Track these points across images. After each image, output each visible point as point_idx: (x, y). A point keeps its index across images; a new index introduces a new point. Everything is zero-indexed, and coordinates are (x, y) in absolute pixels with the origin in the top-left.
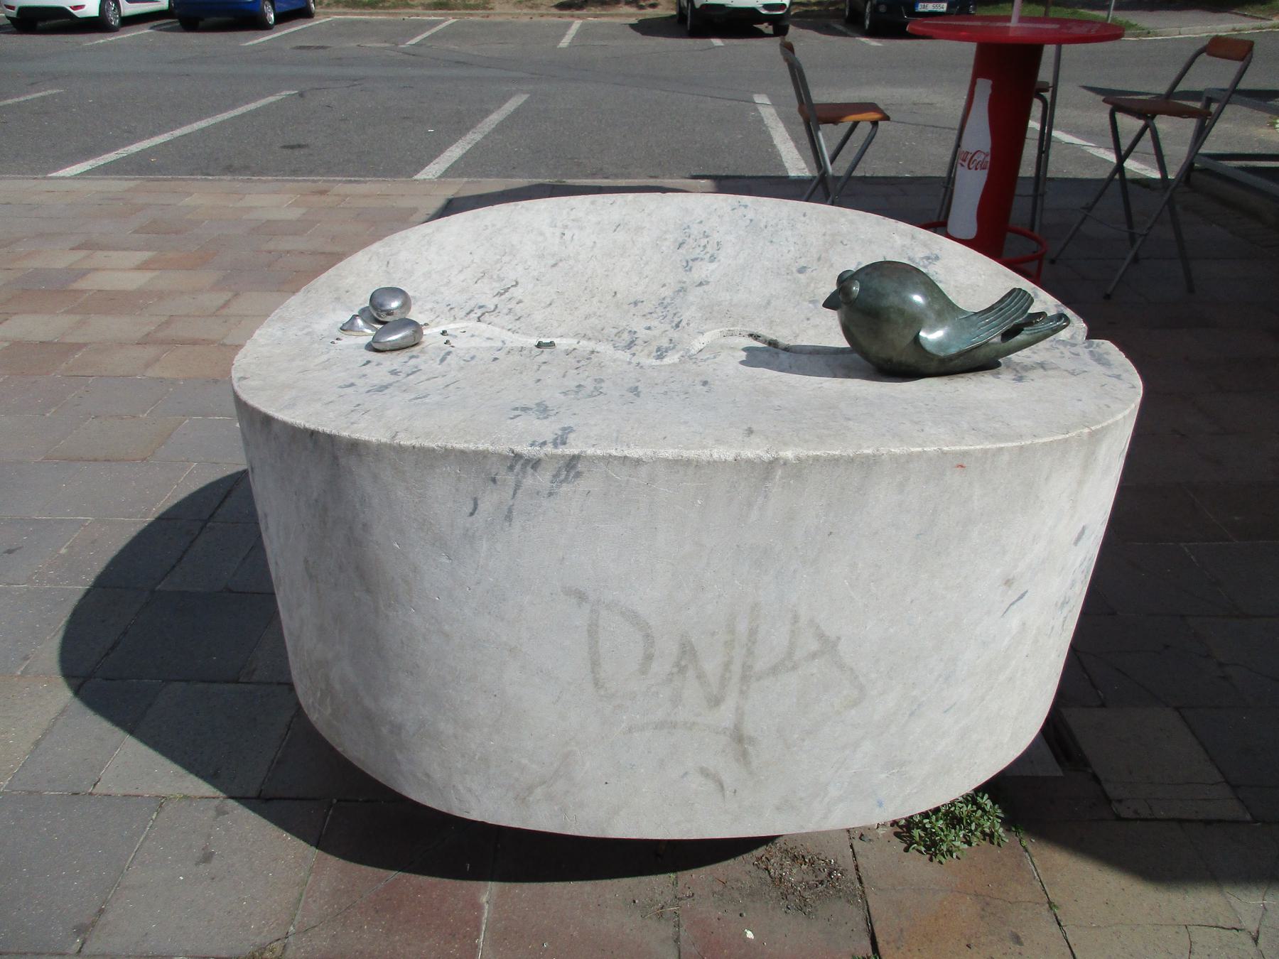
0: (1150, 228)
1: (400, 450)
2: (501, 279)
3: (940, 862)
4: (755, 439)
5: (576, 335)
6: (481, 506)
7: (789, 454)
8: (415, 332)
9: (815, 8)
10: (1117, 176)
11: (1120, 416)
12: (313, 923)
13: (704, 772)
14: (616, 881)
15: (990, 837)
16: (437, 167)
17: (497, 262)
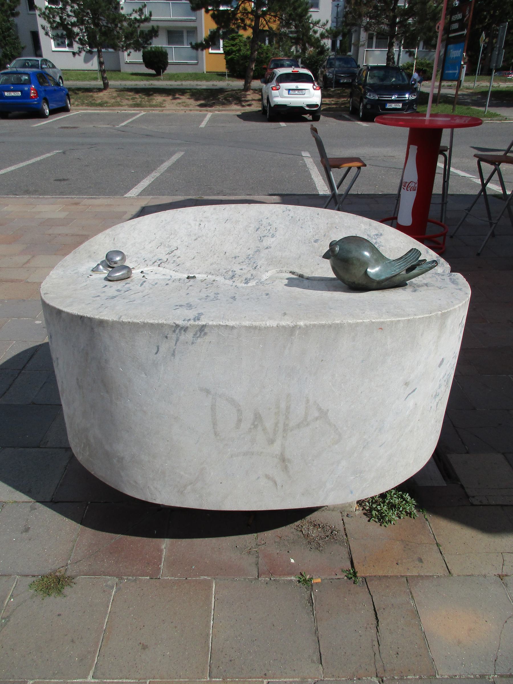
0: (498, 220)
1: (123, 324)
2: (169, 246)
3: (385, 526)
4: (286, 317)
5: (206, 273)
6: (160, 349)
7: (301, 323)
8: (128, 271)
9: (334, 106)
10: (482, 193)
11: (457, 306)
12: (79, 559)
13: (267, 477)
14: (227, 537)
15: (409, 514)
16: (136, 190)
17: (168, 238)
